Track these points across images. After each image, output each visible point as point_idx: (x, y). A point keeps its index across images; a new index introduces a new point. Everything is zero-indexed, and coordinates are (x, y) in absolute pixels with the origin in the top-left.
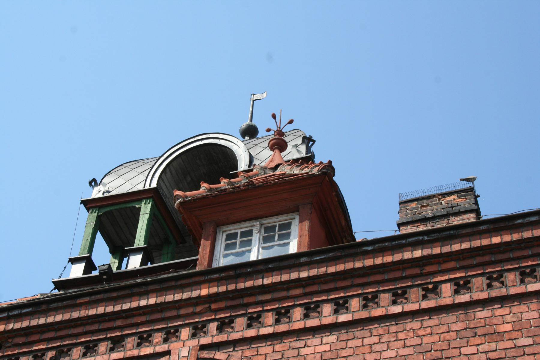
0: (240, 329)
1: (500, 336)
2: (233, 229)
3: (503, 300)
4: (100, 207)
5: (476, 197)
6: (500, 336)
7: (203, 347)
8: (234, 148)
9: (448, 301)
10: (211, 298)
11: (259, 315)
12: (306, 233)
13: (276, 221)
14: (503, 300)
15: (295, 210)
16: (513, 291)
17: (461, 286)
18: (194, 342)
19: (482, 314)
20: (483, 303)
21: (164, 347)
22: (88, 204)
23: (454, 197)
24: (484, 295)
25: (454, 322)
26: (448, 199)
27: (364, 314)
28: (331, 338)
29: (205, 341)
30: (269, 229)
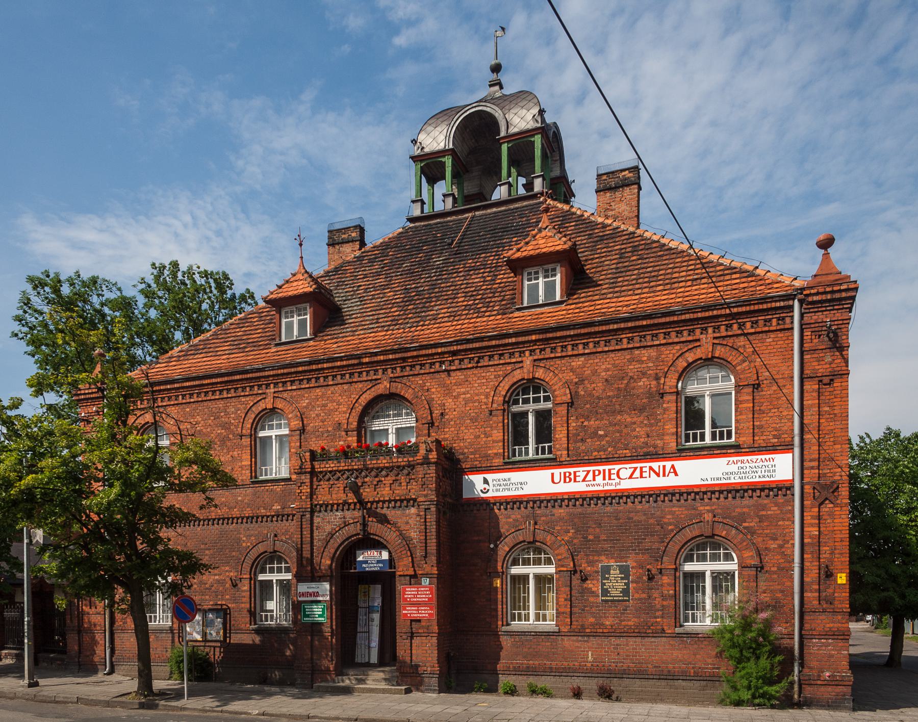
0: (548, 353)
1: (642, 362)
2: (530, 270)
3: (644, 347)
4: (421, 161)
5: (640, 188)
6: (642, 362)
7: (535, 360)
8: (497, 115)
9: (625, 347)
10: (536, 341)
11: (555, 348)
12: (564, 274)
13: (550, 266)
14: (644, 347)
15: (559, 262)
16: (649, 344)
17: (630, 340)
18: (531, 358)
19: (637, 352)
20: (638, 348)
21: (520, 359)
22: (414, 158)
23: (627, 172)
24: (638, 345)
25: (627, 355)
26: (623, 173)
27: (594, 350)
28: (582, 359)
29: (536, 357)
30: (547, 271)
